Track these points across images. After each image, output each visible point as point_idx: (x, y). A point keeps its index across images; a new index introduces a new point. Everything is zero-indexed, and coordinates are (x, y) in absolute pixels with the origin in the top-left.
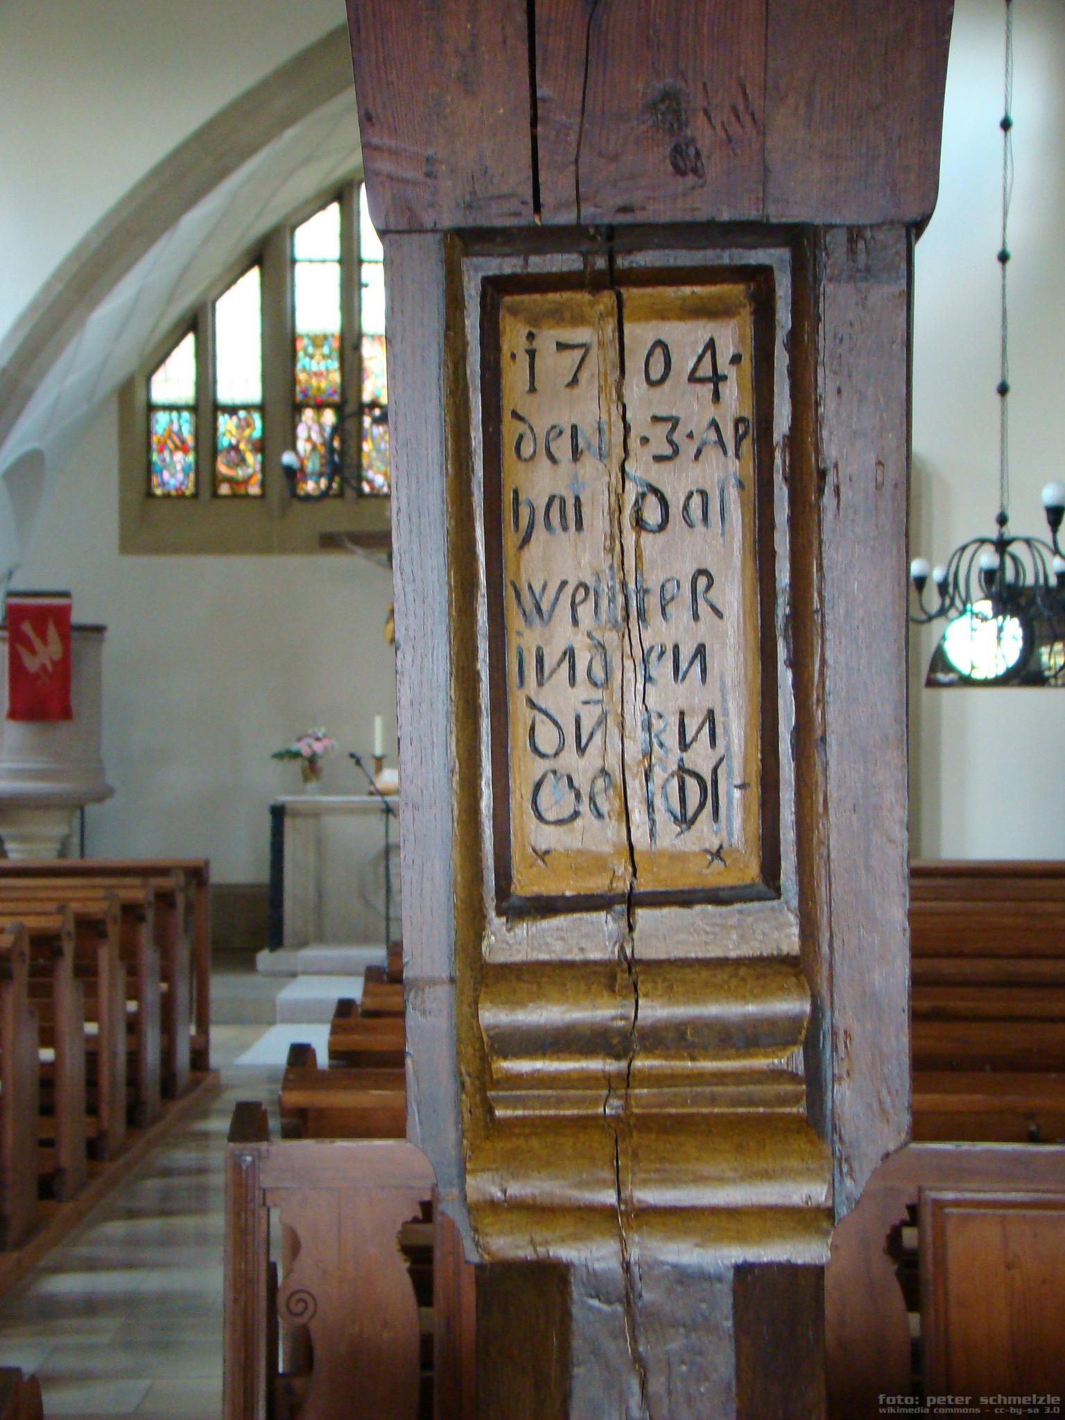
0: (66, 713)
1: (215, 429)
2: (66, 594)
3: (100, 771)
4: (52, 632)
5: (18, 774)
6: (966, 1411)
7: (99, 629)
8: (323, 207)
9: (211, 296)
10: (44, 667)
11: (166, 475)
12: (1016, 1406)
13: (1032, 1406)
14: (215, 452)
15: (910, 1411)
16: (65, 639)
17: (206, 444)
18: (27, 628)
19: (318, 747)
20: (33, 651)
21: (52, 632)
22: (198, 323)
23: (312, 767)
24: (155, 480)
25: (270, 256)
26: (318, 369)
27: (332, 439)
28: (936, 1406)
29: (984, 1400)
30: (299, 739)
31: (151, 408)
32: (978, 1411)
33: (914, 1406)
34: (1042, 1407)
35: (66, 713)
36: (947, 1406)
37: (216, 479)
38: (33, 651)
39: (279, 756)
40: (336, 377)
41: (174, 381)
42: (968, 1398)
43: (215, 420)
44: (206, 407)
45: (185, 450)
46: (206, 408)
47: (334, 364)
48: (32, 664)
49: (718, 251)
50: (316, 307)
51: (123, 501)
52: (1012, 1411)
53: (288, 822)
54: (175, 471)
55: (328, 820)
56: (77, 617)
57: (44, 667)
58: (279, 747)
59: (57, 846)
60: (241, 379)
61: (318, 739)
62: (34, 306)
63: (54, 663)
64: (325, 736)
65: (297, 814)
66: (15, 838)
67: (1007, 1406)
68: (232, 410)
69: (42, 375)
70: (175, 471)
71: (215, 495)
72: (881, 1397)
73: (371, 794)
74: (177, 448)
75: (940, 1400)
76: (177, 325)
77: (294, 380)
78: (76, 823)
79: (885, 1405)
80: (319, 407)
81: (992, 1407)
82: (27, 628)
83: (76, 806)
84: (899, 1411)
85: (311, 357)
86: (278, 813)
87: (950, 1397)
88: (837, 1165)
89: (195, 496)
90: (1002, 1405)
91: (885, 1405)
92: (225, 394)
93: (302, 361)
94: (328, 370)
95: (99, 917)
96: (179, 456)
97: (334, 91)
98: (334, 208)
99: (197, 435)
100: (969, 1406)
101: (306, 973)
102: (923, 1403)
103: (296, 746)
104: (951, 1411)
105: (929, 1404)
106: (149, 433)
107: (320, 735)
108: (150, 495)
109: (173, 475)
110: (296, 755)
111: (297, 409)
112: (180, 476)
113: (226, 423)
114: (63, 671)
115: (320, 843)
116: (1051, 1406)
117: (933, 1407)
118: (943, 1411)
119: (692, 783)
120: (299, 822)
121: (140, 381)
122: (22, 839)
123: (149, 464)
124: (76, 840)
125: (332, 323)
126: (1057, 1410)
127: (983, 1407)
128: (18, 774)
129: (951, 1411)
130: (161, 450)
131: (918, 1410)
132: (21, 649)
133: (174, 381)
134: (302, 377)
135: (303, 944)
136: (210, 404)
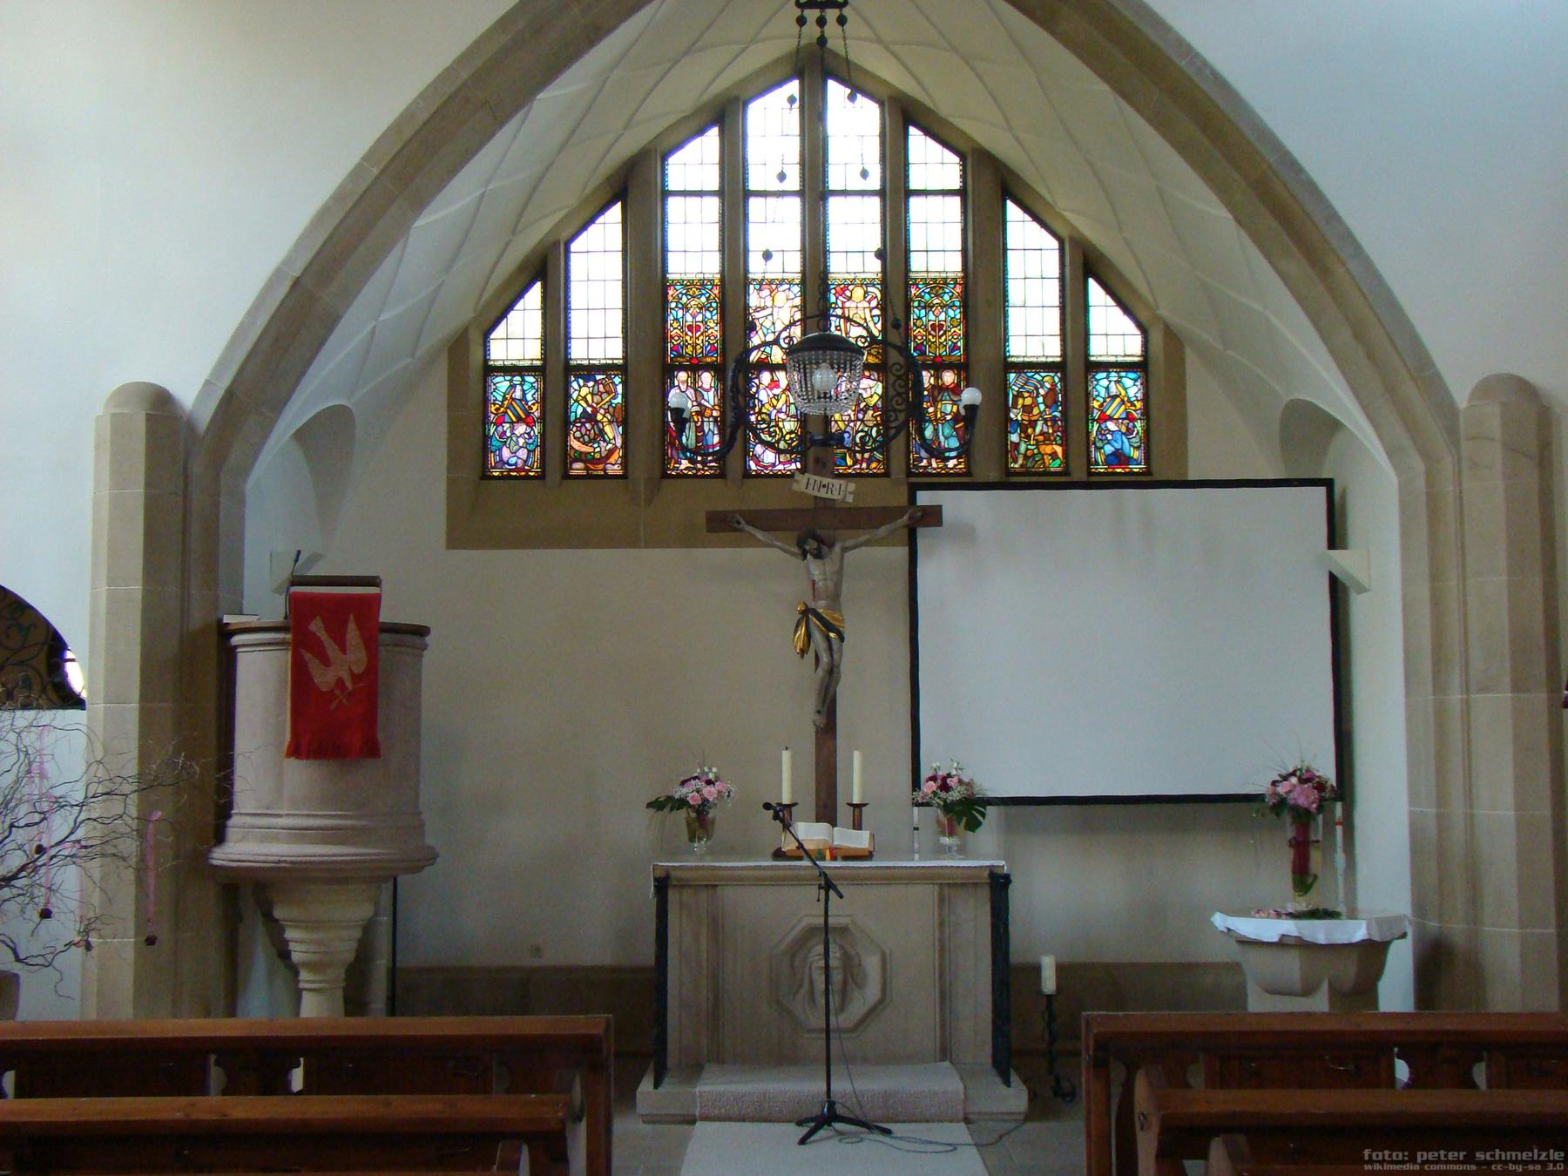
0: (371, 749)
1: (568, 396)
2: (373, 581)
3: (420, 829)
4: (353, 633)
5: (301, 834)
7: (421, 631)
8: (701, 132)
9: (564, 236)
10: (340, 683)
11: (506, 453)
12: (1516, 1162)
13: (1534, 1162)
14: (566, 424)
15: (1398, 1167)
16: (371, 645)
17: (555, 417)
18: (317, 626)
19: (709, 792)
20: (326, 661)
21: (353, 633)
22: (547, 269)
23: (701, 819)
24: (492, 459)
25: (635, 188)
26: (697, 326)
28: (1428, 1162)
29: (1480, 1156)
30: (683, 783)
31: (490, 370)
32: (1474, 1167)
33: (1402, 1162)
34: (1544, 1164)
35: (371, 749)
37: (567, 457)
38: (326, 661)
39: (657, 805)
40: (715, 331)
41: (518, 337)
43: (567, 385)
44: (555, 367)
45: (527, 420)
46: (556, 370)
47: (713, 318)
48: (323, 678)
50: (692, 246)
51: (452, 484)
52: (1511, 1167)
53: (672, 896)
54: (516, 447)
55: (729, 894)
56: (385, 616)
57: (340, 683)
58: (659, 793)
59: (357, 933)
60: (598, 332)
61: (709, 782)
62: (338, 197)
63: (356, 678)
64: (717, 779)
65: (684, 885)
66: (298, 924)
67: (1506, 1162)
68: (588, 371)
69: (348, 296)
70: (516, 447)
71: (567, 476)
72: (1367, 1152)
73: (779, 854)
74: (520, 420)
75: (1431, 1156)
76: (521, 269)
77: (664, 337)
78: (386, 900)
79: (1371, 1161)
80: (695, 368)
81: (1489, 1164)
82: (317, 626)
83: (385, 879)
84: (1387, 1167)
85: (685, 308)
86: (663, 885)
87: (1442, 1153)
89: (541, 477)
90: (1500, 1161)
92: (579, 352)
93: (675, 314)
94: (704, 322)
96: (521, 429)
98: (713, 134)
99: (543, 401)
100: (1463, 1163)
101: (705, 1118)
102: (1413, 1160)
103: (679, 792)
104: (1443, 1167)
106: (485, 402)
107: (711, 776)
108: (485, 476)
109: (514, 453)
110: (682, 803)
111: (668, 371)
112: (523, 454)
113: (580, 390)
114: (368, 686)
115: (716, 926)
116: (1555, 1163)
117: (1424, 1163)
118: (1434, 1167)
120: (686, 895)
121: (475, 336)
122: (311, 925)
123: (486, 438)
124: (385, 919)
125: (710, 266)
126: (1561, 1167)
127: (1479, 1164)
128: (301, 834)
129: (1443, 1167)
130: (499, 423)
132: (308, 656)
133: (518, 337)
134: (673, 331)
135: (694, 1070)
136: (561, 368)
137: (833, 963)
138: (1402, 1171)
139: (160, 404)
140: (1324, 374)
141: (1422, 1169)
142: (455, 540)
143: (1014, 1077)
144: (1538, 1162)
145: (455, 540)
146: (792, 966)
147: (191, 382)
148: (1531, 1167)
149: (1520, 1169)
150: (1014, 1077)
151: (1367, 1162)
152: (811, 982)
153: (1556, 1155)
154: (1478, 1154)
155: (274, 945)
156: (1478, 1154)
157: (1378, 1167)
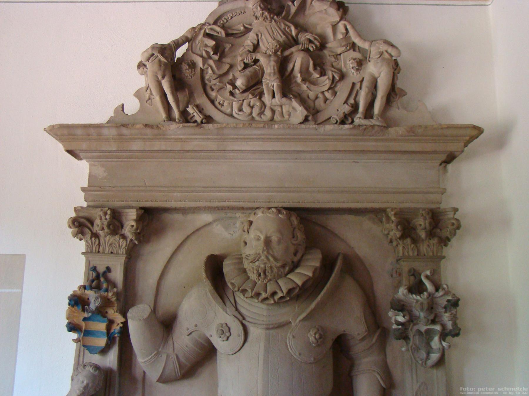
6: (492, 393)
15: (472, 393)
27: (278, 51)
28: (482, 391)
36: (485, 391)
42: (493, 389)
49: (108, 220)
67: (508, 392)
72: (461, 388)
75: (483, 389)
87: (487, 388)
88: (218, 69)
91: (463, 391)
95: (83, 380)
97: (104, 322)
100: (494, 391)
102: (477, 390)
105: (479, 391)
116: (525, 391)
118: (484, 393)
119: (198, 117)
126: (526, 393)
129: (487, 393)
131: (475, 393)
139: (344, 112)
140: (7, 291)
143: (341, 10)
147: (346, 113)
150: (341, 10)
151: (461, 391)
152: (297, 236)
154: (499, 389)
155: (68, 318)
156: (499, 389)
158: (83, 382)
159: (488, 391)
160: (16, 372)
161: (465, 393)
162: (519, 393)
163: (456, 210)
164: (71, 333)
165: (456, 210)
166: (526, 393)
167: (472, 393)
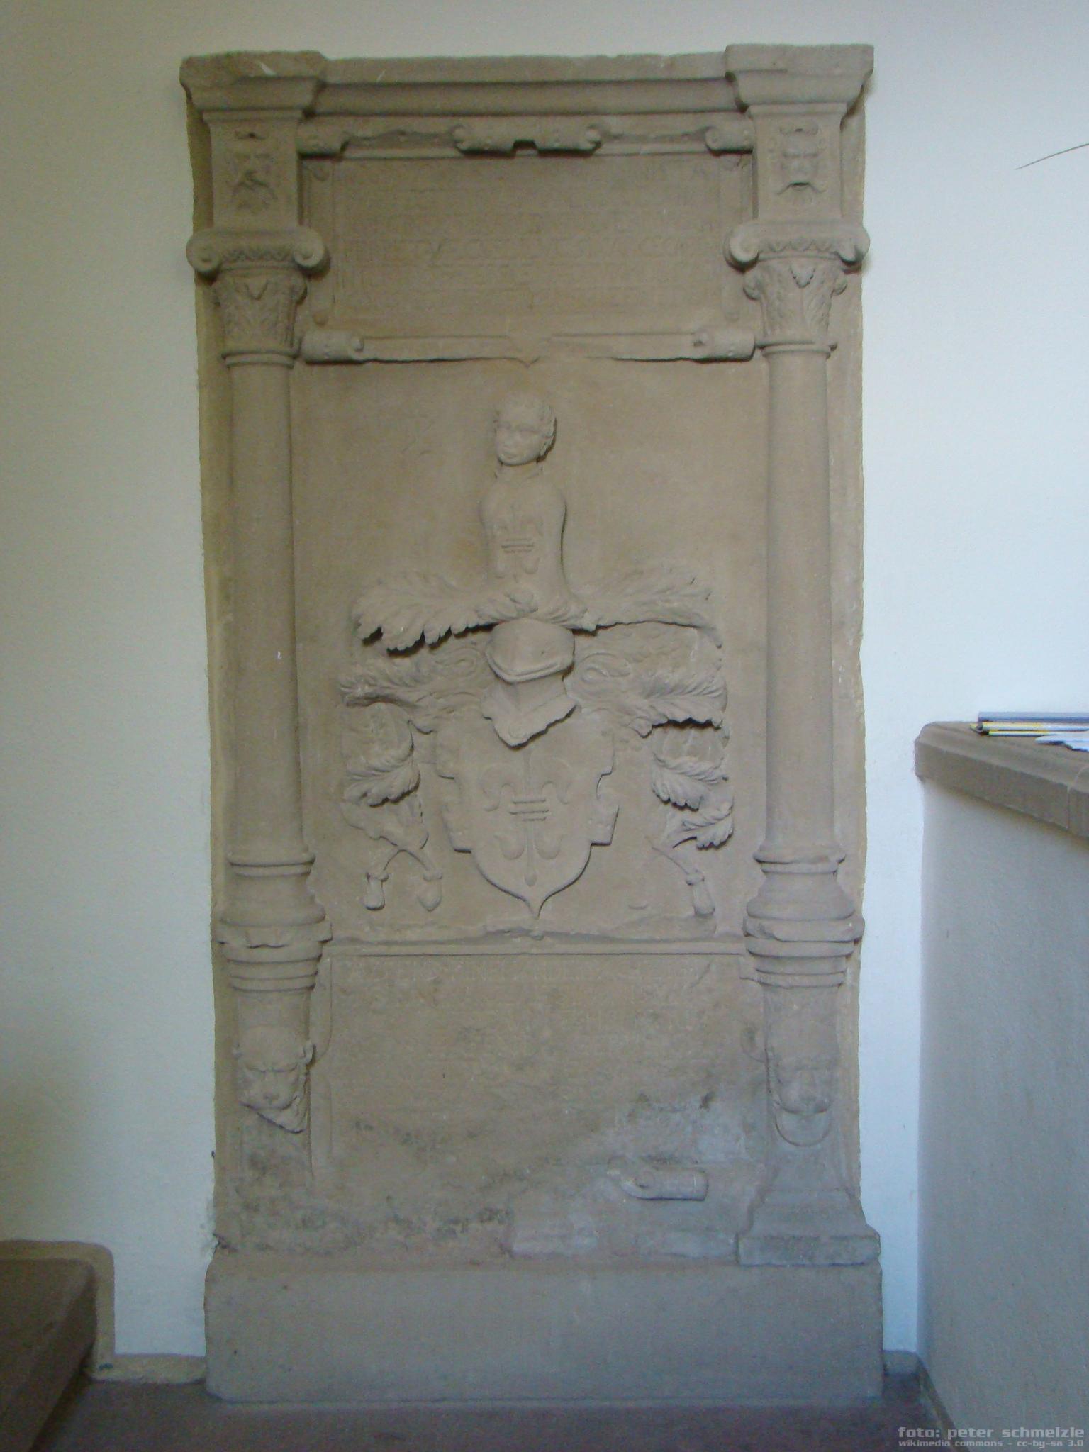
12: (1040, 1439)
13: (1054, 1439)
15: (931, 1444)
34: (1065, 1441)
42: (989, 1432)
52: (1053, 1444)
67: (1030, 1439)
72: (901, 1430)
79: (905, 1438)
84: (919, 1444)
90: (1024, 1439)
91: (905, 1438)
116: (1075, 1439)
126: (1080, 1444)
127: (1005, 1440)
131: (938, 1444)
137: (540, 951)
138: (934, 1448)
141: (1048, 1447)
142: (868, 51)
144: (1060, 1439)
145: (868, 51)
146: (307, 1074)
148: (1053, 1444)
149: (1043, 1445)
153: (1077, 1433)
154: (1004, 1432)
156: (1004, 1432)
157: (911, 1443)
158: (326, 346)
159: (925, 1439)
160: (204, 636)
161: (968, 1444)
162: (1060, 1444)
163: (202, 1226)
164: (212, 1161)
165: (202, 1226)
166: (1080, 1444)
167: (931, 1444)
